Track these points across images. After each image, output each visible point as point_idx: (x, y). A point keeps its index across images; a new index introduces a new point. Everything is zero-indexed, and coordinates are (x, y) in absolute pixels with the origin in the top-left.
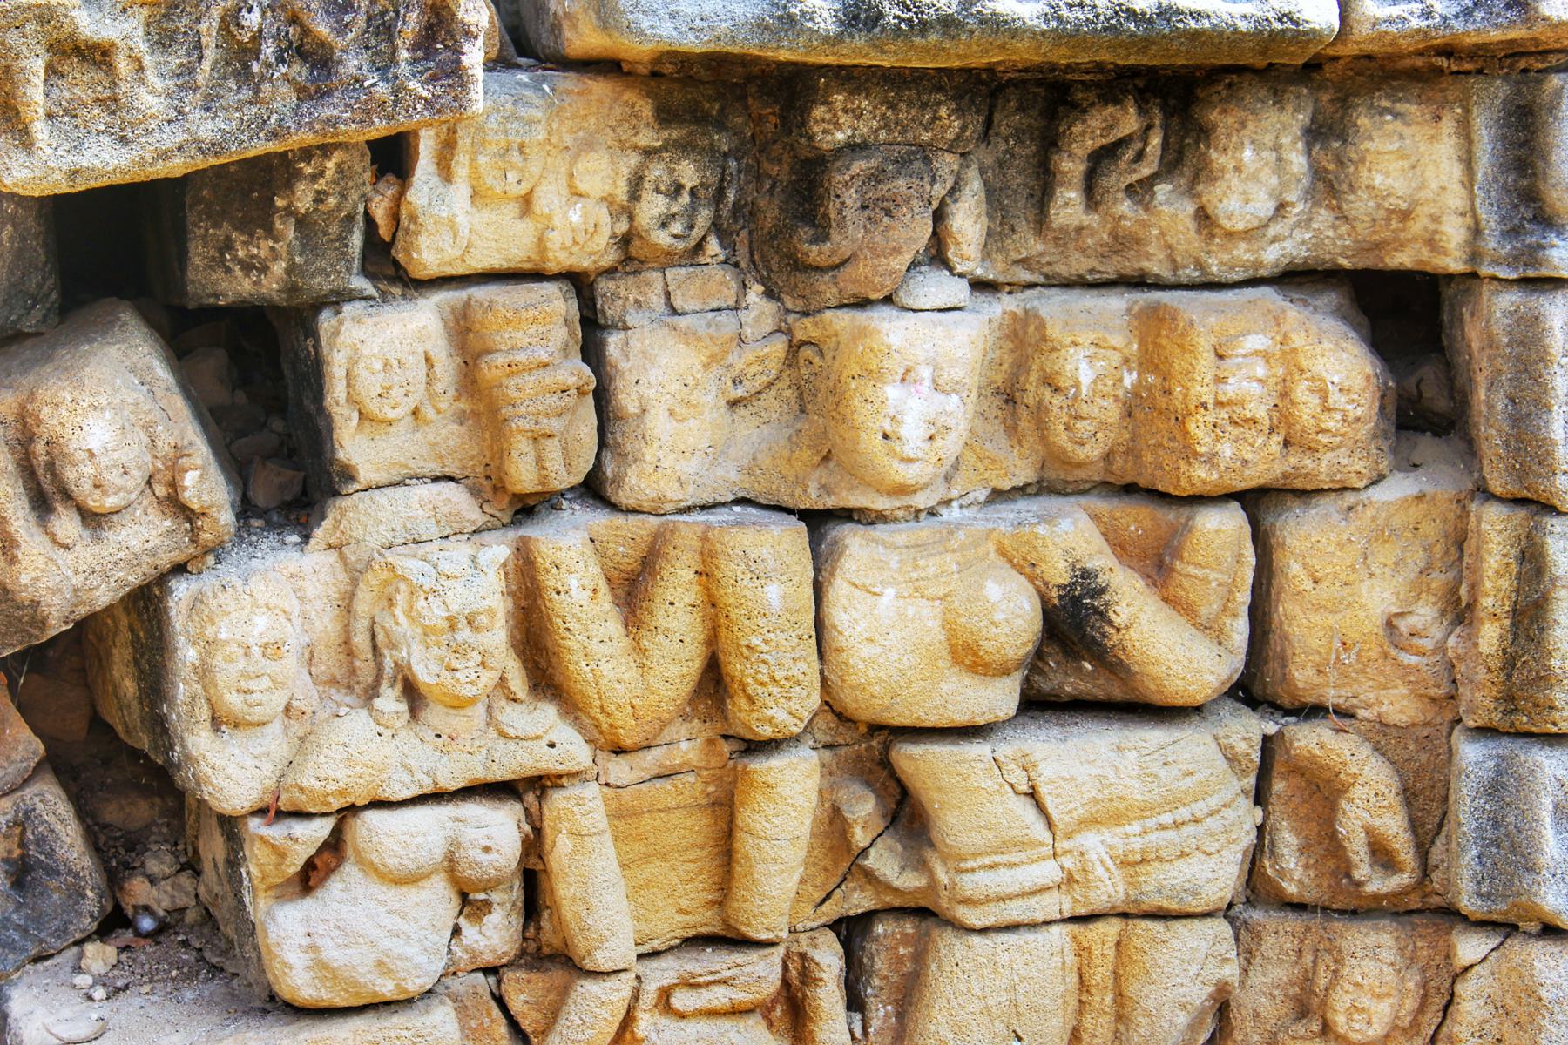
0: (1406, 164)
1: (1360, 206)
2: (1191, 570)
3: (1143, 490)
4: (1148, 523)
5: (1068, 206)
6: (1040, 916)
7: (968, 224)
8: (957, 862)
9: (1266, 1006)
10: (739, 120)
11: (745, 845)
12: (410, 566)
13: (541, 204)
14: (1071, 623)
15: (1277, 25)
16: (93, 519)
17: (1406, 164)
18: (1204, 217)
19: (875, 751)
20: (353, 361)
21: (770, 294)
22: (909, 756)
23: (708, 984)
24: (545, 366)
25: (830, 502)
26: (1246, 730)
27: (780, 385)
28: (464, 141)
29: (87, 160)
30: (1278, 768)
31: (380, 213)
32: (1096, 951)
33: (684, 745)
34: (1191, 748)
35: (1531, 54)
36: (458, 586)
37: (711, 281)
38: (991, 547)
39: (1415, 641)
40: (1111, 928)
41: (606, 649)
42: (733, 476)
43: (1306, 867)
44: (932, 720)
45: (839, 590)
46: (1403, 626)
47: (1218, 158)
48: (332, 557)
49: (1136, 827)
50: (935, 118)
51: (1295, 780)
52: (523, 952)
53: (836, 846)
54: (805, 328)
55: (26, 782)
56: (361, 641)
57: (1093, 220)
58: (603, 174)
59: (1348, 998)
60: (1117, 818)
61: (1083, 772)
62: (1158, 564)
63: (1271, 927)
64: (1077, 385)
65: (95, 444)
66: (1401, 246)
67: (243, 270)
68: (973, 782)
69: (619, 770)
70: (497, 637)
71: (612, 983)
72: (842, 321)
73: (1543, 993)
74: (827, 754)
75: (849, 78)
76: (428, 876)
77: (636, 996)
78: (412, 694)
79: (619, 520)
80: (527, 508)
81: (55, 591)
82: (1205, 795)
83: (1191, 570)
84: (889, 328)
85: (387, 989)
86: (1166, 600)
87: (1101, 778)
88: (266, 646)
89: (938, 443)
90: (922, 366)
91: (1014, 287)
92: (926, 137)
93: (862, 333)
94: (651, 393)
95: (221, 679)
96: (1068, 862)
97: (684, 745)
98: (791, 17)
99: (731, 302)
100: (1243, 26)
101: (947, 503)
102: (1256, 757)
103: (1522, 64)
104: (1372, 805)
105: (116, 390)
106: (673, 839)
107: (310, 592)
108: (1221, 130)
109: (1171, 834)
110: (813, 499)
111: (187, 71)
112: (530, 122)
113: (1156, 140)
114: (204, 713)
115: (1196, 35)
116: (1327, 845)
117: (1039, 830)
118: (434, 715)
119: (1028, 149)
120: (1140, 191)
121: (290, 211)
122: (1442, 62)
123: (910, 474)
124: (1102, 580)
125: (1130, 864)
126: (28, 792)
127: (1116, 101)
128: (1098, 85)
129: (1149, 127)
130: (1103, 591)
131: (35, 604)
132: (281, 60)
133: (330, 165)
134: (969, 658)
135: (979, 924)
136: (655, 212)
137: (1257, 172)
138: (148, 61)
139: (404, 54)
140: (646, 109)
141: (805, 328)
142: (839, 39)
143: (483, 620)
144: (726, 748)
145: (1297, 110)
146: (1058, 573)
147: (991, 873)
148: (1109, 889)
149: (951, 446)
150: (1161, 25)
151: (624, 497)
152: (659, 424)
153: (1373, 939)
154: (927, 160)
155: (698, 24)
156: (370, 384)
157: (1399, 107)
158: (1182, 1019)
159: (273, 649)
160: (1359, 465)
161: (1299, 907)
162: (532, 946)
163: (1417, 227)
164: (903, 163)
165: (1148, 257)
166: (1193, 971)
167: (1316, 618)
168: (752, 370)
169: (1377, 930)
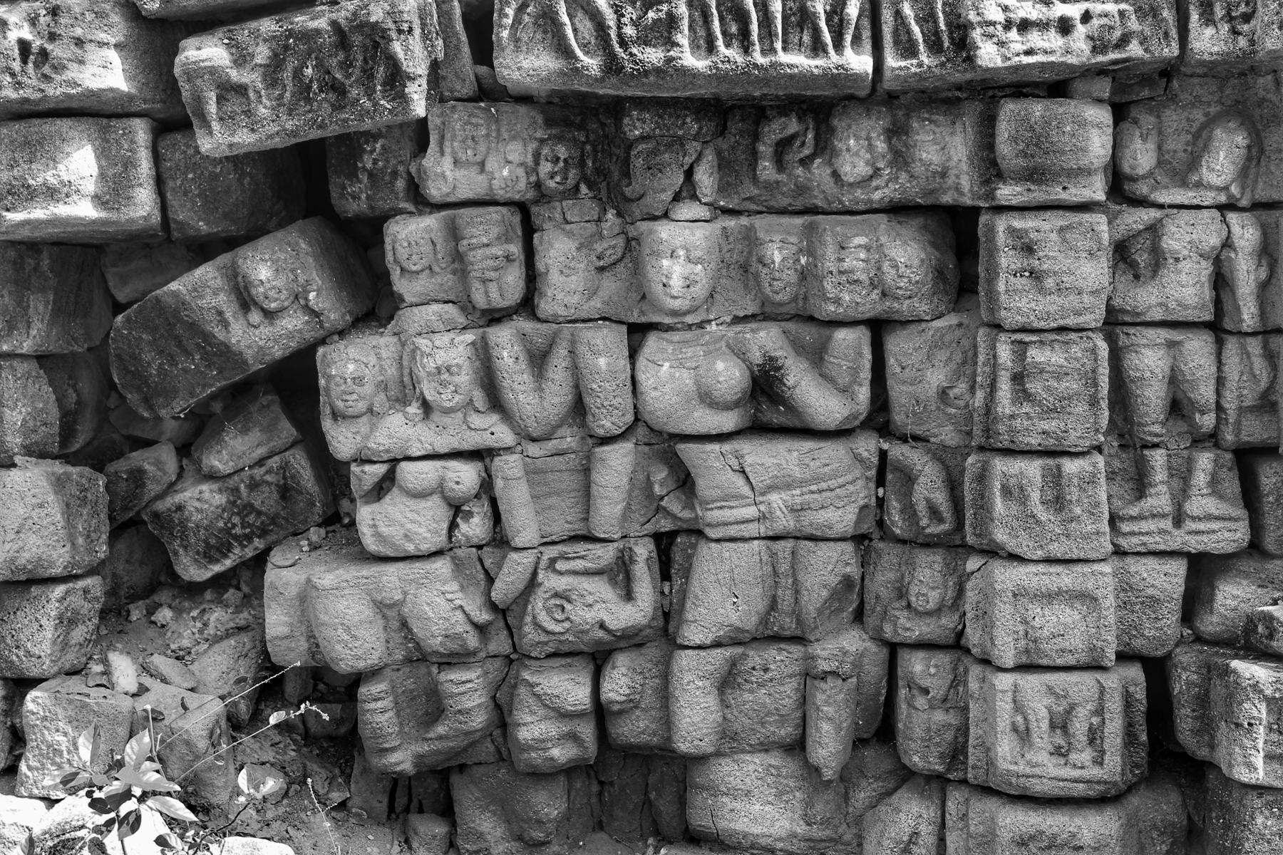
0: (938, 147)
1: (918, 169)
2: (832, 359)
3: (808, 320)
4: (816, 336)
5: (766, 169)
6: (747, 535)
7: (705, 179)
8: (705, 503)
9: (884, 593)
10: (595, 126)
11: (594, 490)
12: (423, 343)
13: (488, 167)
14: (765, 385)
15: (835, 71)
16: (269, 315)
17: (938, 147)
18: (836, 175)
19: (665, 445)
20: (394, 242)
21: (619, 215)
22: (688, 451)
23: (574, 558)
24: (488, 245)
25: (644, 320)
26: (867, 445)
27: (626, 260)
28: (448, 136)
29: (236, 139)
30: (889, 468)
31: (413, 170)
32: (780, 555)
33: (569, 439)
34: (833, 452)
35: (994, 88)
36: (442, 353)
37: (582, 209)
38: (723, 344)
39: (957, 402)
40: (789, 544)
41: (522, 388)
42: (599, 305)
43: (904, 520)
44: (689, 431)
45: (642, 362)
46: (951, 393)
47: (839, 145)
48: (395, 339)
49: (798, 492)
50: (684, 123)
51: (898, 474)
52: (494, 539)
53: (642, 491)
54: (632, 232)
55: (287, 449)
56: (406, 379)
57: (782, 177)
58: (517, 152)
59: (917, 589)
60: (788, 486)
61: (769, 461)
62: (817, 356)
63: (886, 551)
64: (773, 262)
65: (263, 277)
66: (945, 193)
67: (354, 199)
68: (709, 463)
69: (533, 450)
70: (464, 378)
71: (525, 554)
72: (643, 226)
73: (996, 586)
74: (647, 449)
75: (640, 103)
76: (431, 494)
77: (537, 563)
78: (427, 407)
79: (539, 326)
80: (495, 317)
81: (249, 347)
82: (836, 477)
83: (832, 359)
84: (664, 231)
85: (411, 548)
86: (823, 376)
87: (779, 465)
88: (354, 378)
89: (692, 289)
90: (683, 252)
91: (750, 213)
92: (680, 133)
93: (651, 232)
94: (550, 262)
95: (333, 394)
96: (762, 508)
97: (569, 439)
98: (577, 69)
99: (596, 218)
100: (816, 71)
101: (709, 322)
102: (875, 460)
103: (990, 93)
104: (929, 486)
105: (274, 253)
106: (563, 486)
107: (384, 355)
108: (839, 129)
109: (816, 496)
110: (635, 318)
111: (281, 97)
112: (477, 125)
113: (810, 136)
114: (328, 411)
115: (792, 76)
116: (909, 511)
117: (746, 490)
118: (436, 416)
119: (746, 141)
120: (805, 162)
121: (364, 168)
122: (958, 94)
123: (676, 304)
124: (780, 362)
125: (795, 510)
126: (287, 454)
127: (786, 115)
128: (778, 107)
129: (807, 129)
130: (780, 368)
131: (241, 353)
132: (321, 91)
133: (378, 146)
134: (707, 399)
135: (714, 536)
136: (546, 170)
137: (859, 151)
138: (263, 92)
139: (379, 88)
140: (540, 120)
141: (630, 229)
142: (602, 80)
143: (455, 369)
144: (590, 441)
145: (878, 119)
146: (757, 357)
147: (721, 512)
148: (784, 522)
149: (699, 291)
150: (772, 71)
151: (541, 315)
152: (555, 277)
153: (931, 558)
154: (682, 145)
155: (531, 72)
156: (403, 253)
157: (934, 117)
158: (825, 593)
159: (358, 380)
160: (925, 308)
161: (904, 542)
162: (498, 537)
163: (951, 181)
164: (669, 146)
165: (816, 197)
166: (830, 568)
167: (904, 388)
168: (609, 252)
169: (934, 553)
